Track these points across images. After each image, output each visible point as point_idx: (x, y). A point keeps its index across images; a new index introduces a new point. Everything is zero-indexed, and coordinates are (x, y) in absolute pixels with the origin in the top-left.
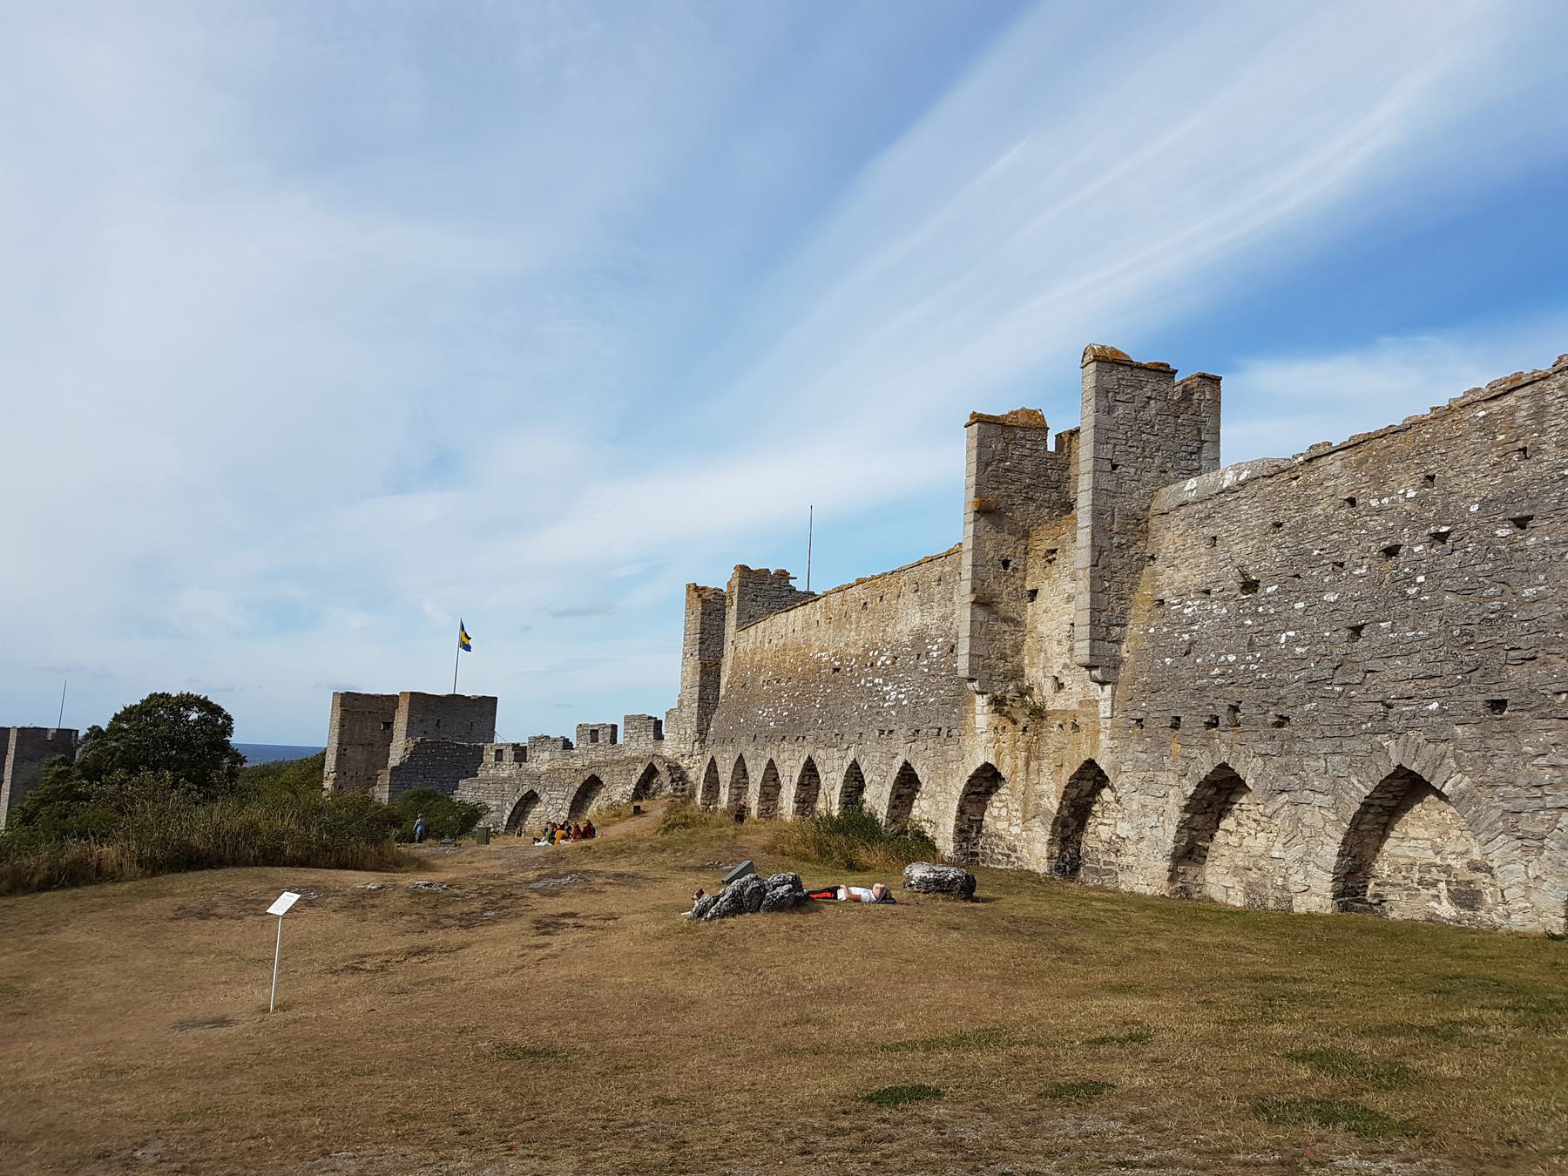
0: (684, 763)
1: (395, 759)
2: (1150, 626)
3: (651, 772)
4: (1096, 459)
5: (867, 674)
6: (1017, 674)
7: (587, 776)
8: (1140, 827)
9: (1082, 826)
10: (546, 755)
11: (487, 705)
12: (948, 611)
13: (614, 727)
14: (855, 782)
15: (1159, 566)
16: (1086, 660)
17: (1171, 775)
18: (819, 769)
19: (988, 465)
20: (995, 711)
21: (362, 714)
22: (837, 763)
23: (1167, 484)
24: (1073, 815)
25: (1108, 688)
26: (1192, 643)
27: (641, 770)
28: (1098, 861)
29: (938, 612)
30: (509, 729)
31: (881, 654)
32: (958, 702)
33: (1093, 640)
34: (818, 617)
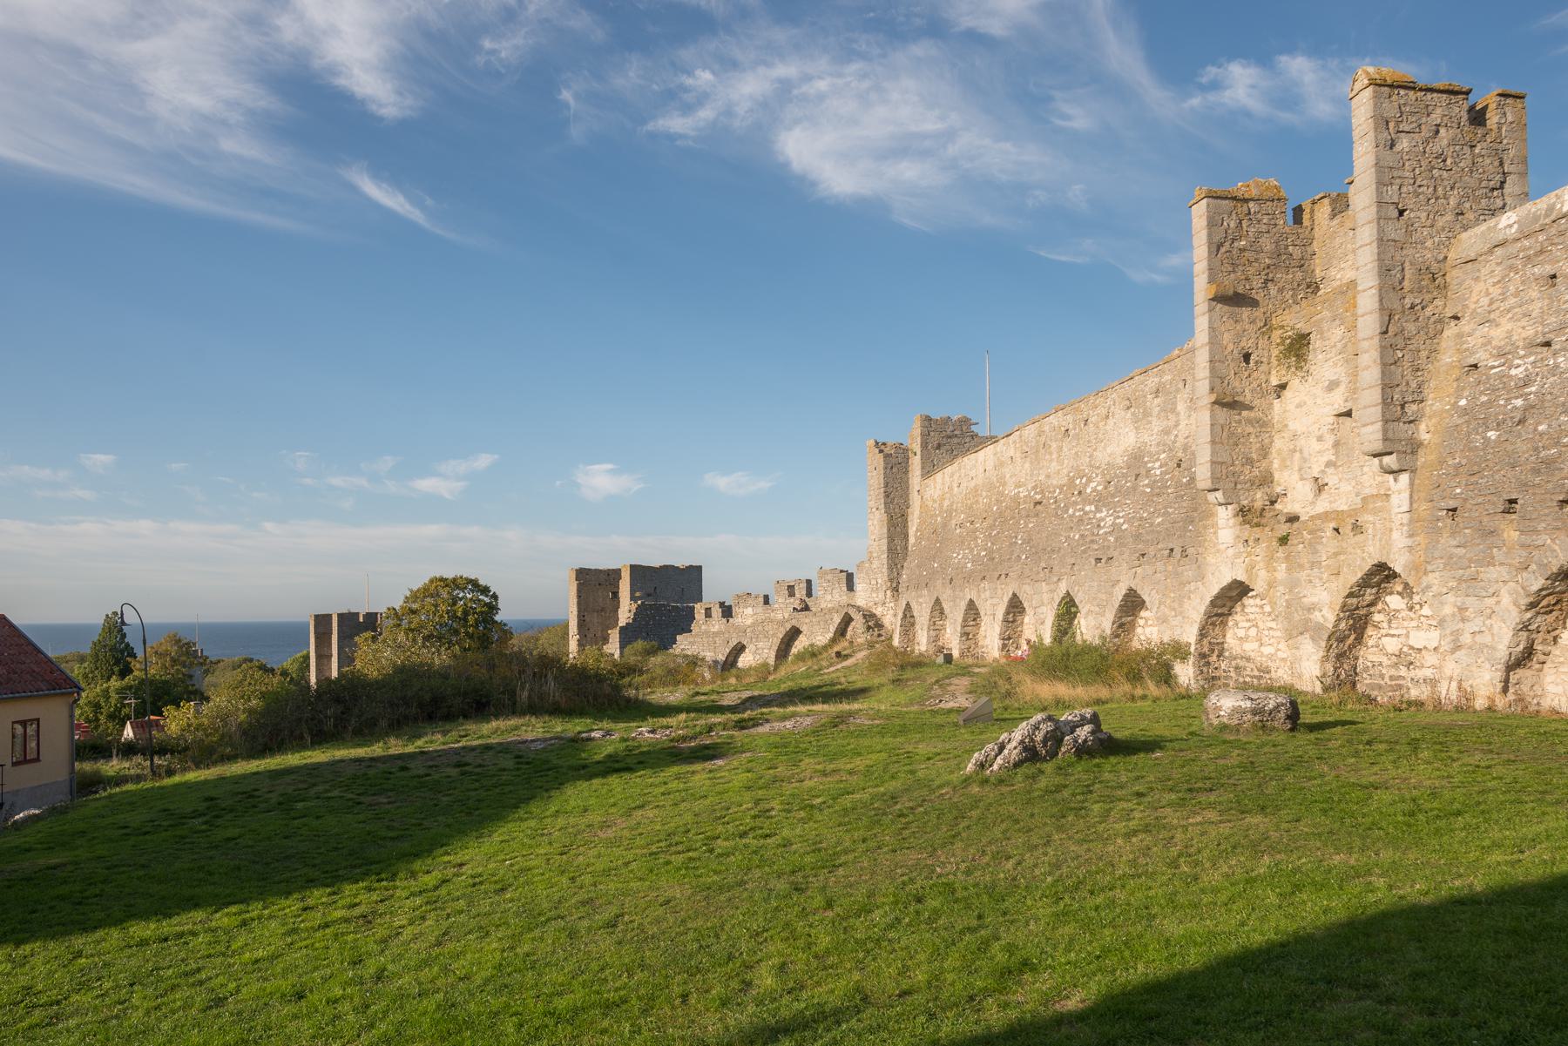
0: (878, 611)
1: (622, 622)
2: (1460, 397)
3: (847, 620)
4: (1380, 203)
5: (1075, 503)
6: (1266, 480)
7: (788, 627)
8: (1457, 634)
9: (1359, 639)
10: (749, 611)
11: (695, 572)
12: (1171, 423)
13: (809, 582)
14: (1068, 611)
15: (1466, 325)
16: (1378, 446)
17: (1503, 570)
18: (1026, 605)
19: (1220, 246)
20: (1245, 522)
21: (595, 586)
22: (1046, 597)
23: (1465, 228)
24: (1353, 628)
25: (1404, 478)
26: (1528, 408)
27: (837, 619)
28: (1382, 676)
29: (1157, 425)
30: (713, 589)
31: (1090, 480)
32: (1195, 516)
33: (1386, 421)
34: (1012, 453)
